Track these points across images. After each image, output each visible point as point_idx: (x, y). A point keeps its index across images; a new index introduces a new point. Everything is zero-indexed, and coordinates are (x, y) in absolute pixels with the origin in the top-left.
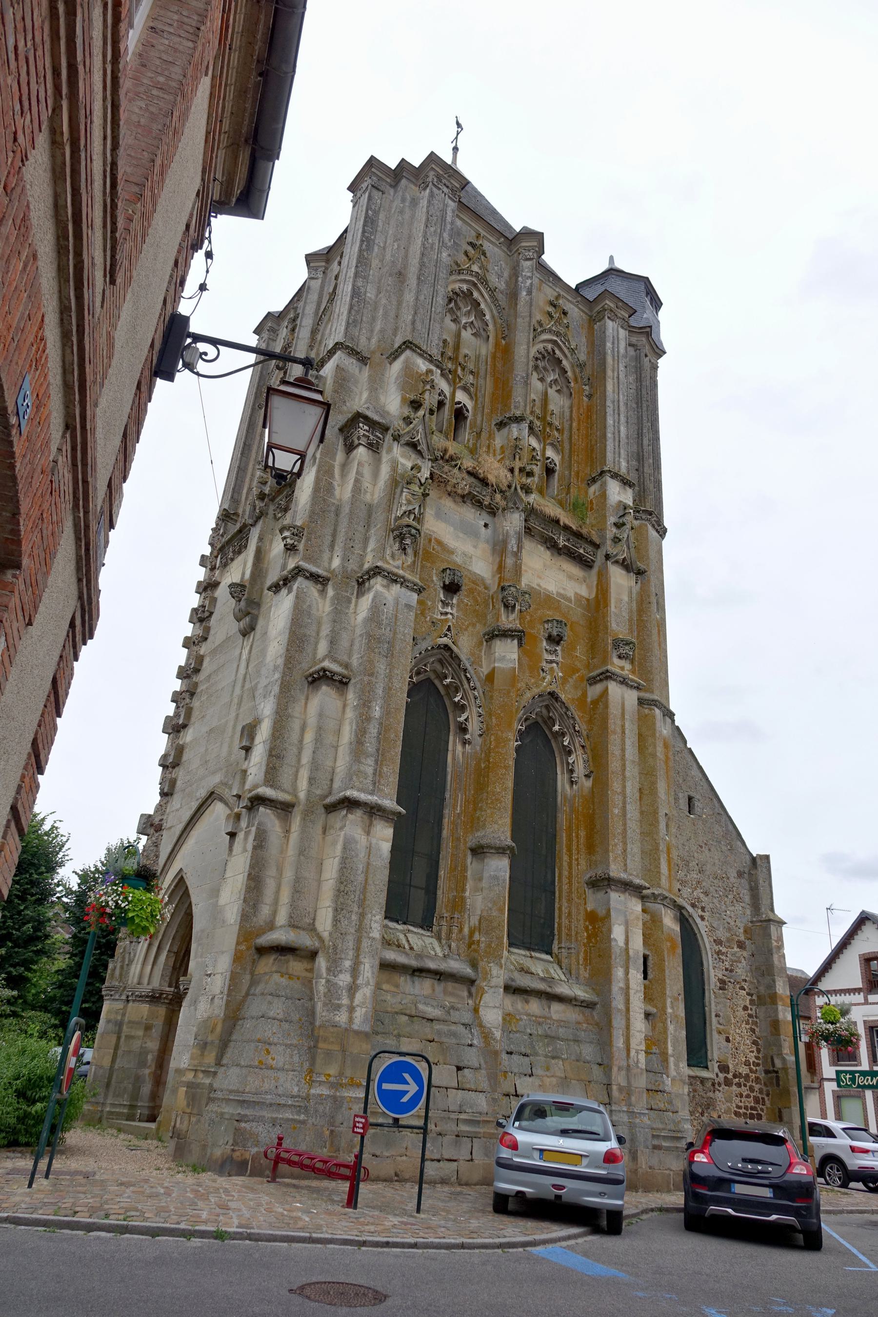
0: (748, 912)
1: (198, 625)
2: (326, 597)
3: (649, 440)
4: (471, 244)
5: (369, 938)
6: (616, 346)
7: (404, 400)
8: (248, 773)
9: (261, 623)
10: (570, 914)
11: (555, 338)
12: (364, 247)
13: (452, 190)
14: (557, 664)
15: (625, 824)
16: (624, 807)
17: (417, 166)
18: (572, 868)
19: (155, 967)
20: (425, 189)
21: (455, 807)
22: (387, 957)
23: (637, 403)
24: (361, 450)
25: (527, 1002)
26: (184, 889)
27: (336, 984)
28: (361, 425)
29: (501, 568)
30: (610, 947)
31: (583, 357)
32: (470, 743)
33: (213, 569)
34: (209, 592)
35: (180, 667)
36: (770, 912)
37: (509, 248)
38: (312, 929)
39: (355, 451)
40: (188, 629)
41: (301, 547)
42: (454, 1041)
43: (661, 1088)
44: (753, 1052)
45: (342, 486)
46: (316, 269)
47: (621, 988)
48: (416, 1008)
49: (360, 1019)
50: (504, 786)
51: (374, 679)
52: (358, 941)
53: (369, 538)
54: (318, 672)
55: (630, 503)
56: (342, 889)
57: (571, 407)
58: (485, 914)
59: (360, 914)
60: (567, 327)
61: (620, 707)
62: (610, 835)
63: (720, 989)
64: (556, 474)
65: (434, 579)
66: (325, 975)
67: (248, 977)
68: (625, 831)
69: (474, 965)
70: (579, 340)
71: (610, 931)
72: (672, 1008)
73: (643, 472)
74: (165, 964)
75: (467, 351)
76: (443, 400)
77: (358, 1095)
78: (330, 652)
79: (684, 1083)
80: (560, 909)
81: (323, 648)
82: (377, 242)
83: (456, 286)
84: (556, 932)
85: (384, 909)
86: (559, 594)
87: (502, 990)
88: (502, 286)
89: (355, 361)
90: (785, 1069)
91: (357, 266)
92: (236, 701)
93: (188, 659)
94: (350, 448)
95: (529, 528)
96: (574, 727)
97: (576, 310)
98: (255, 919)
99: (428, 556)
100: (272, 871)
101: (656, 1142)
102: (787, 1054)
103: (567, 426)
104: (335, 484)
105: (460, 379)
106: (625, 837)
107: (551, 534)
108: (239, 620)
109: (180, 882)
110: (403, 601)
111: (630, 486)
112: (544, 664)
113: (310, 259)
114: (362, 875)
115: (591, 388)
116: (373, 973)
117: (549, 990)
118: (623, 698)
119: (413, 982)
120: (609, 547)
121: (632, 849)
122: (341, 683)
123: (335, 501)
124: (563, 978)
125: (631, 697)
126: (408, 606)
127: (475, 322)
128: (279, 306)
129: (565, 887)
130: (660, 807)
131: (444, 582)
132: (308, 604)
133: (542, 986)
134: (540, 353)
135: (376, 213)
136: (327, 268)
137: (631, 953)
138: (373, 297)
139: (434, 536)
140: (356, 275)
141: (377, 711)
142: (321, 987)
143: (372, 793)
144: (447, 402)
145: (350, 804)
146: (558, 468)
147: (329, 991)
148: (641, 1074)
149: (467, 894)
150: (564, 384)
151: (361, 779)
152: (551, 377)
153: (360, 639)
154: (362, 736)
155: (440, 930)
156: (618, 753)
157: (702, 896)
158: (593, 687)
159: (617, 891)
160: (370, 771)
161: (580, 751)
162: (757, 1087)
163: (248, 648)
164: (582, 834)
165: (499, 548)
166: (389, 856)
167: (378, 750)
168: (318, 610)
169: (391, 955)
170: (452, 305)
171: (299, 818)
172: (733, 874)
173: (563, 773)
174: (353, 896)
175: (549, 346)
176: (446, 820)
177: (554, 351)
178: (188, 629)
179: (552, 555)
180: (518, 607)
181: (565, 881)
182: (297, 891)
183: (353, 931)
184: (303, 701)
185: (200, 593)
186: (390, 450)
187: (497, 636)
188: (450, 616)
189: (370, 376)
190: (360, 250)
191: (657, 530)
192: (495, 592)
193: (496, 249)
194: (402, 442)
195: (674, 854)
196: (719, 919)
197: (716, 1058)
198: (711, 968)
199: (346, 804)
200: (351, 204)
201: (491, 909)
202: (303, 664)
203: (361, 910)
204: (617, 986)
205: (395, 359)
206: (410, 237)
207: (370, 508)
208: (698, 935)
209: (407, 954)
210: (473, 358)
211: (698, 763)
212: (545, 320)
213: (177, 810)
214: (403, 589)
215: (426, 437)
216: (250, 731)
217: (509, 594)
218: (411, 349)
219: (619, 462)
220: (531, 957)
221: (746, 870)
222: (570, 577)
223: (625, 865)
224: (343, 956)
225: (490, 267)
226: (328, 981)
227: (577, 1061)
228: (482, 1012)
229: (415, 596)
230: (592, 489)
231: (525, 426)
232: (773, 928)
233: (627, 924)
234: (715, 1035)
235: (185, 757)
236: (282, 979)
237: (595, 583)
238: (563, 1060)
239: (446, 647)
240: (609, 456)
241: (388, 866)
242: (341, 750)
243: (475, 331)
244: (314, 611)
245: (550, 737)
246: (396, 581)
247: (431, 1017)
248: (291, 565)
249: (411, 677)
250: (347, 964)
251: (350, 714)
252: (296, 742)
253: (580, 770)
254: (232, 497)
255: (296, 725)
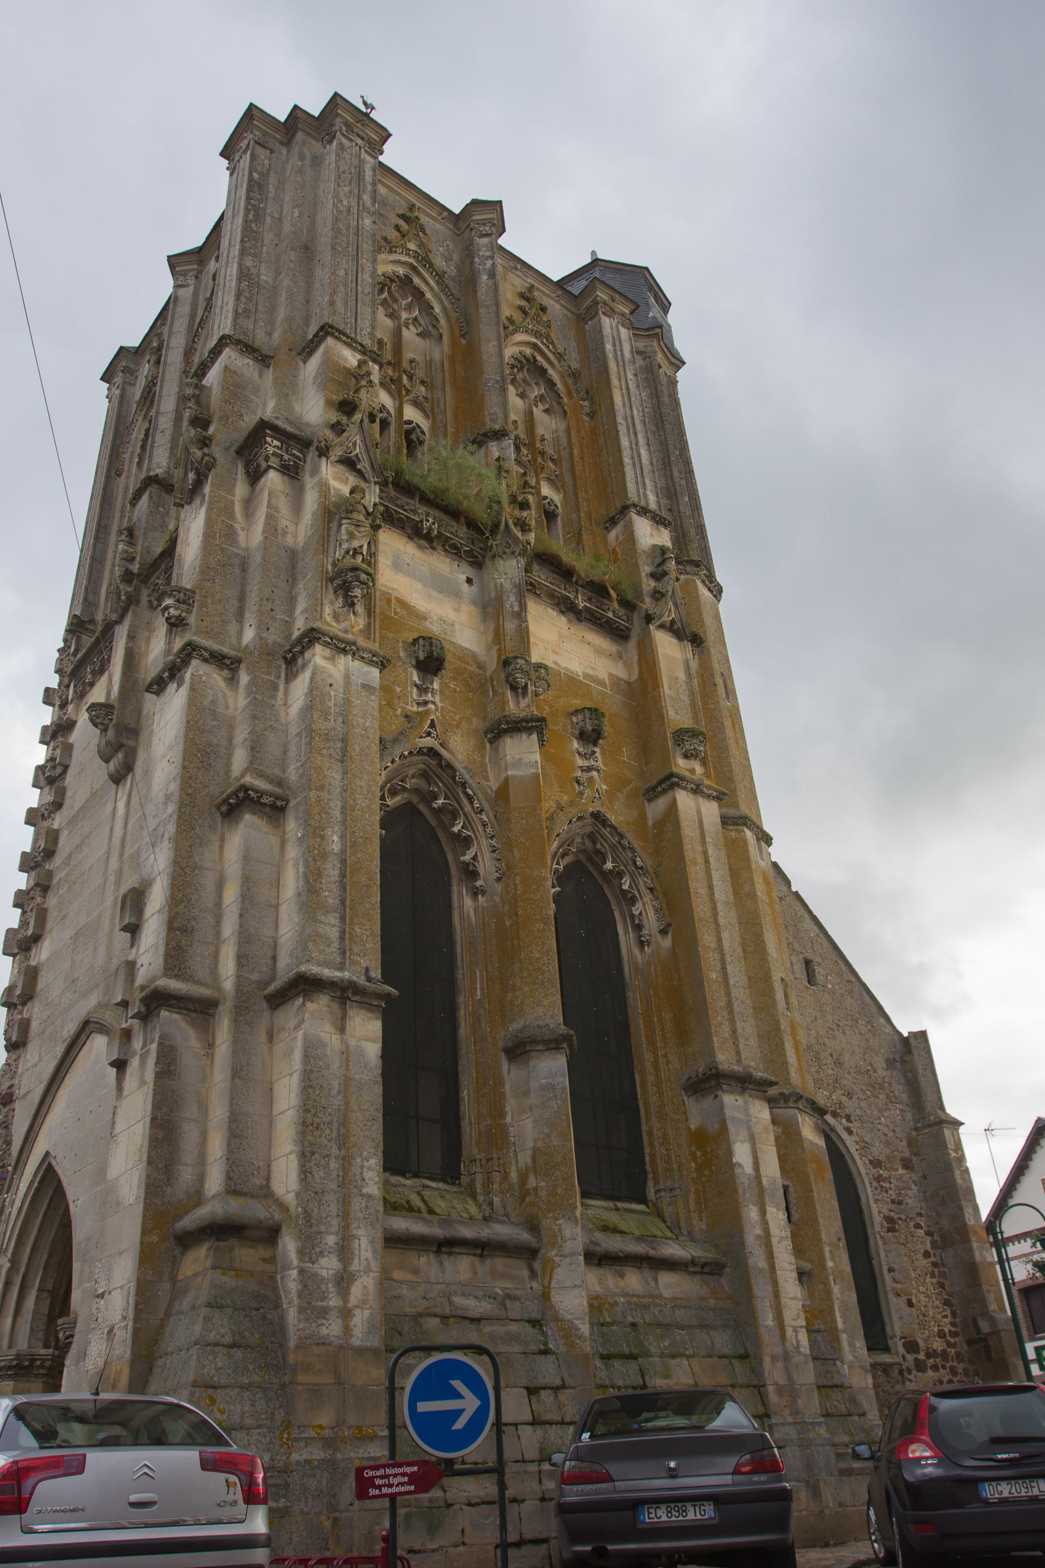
0: (909, 1116)
1: (47, 789)
2: (237, 688)
3: (681, 473)
4: (402, 216)
5: (363, 1196)
6: (618, 348)
7: (329, 403)
8: (138, 965)
9: (141, 756)
10: (665, 1137)
11: (534, 340)
12: (251, 217)
13: (370, 143)
14: (598, 771)
15: (728, 994)
16: (724, 969)
17: (316, 115)
18: (658, 1070)
19: (19, 1319)
20: (330, 142)
21: (473, 990)
22: (395, 1226)
23: (656, 425)
24: (272, 476)
25: (622, 1276)
26: (55, 1184)
27: (316, 1274)
28: (269, 439)
29: (498, 636)
30: (733, 1176)
31: (575, 365)
32: (484, 893)
33: (63, 706)
34: (60, 739)
35: (24, 853)
36: (939, 1112)
37: (455, 225)
38: (266, 1193)
39: (263, 480)
40: (33, 798)
41: (192, 619)
42: (517, 1348)
43: (836, 1381)
44: (946, 1316)
45: (247, 529)
46: (185, 274)
47: (758, 1236)
48: (451, 1303)
49: (363, 1325)
50: (542, 950)
51: (324, 795)
52: (345, 1202)
53: (296, 596)
54: (235, 794)
55: (669, 544)
56: (309, 1120)
57: (568, 431)
58: (540, 1145)
59: (344, 1159)
60: (549, 326)
61: (697, 825)
62: (710, 1012)
63: (889, 1230)
64: (559, 519)
65: (402, 654)
66: (295, 1262)
67: (167, 1286)
68: (729, 1004)
69: (534, 1228)
70: (566, 342)
71: (730, 1153)
72: (833, 1259)
73: (679, 512)
74: (35, 1312)
75: (412, 356)
76: (386, 419)
77: (372, 1454)
78: (251, 763)
79: (866, 1371)
80: (650, 1133)
81: (239, 760)
82: (268, 211)
83: (389, 268)
84: (648, 1168)
85: (381, 1148)
86: (586, 675)
87: (582, 1258)
88: (452, 270)
89: (251, 362)
90: (996, 1333)
91: (242, 241)
92: (112, 879)
93: (35, 840)
94: (254, 476)
95: (531, 584)
96: (635, 862)
97: (558, 306)
98: (169, 1190)
99: (389, 622)
100: (190, 1111)
101: (843, 1465)
102: (994, 1311)
103: (565, 454)
104: (238, 526)
105: (408, 391)
106: (731, 1012)
107: (565, 593)
108: (107, 761)
109: (48, 1175)
110: (357, 680)
111: (665, 526)
112: (579, 773)
113: (175, 262)
114: (341, 1097)
115: (592, 404)
116: (374, 1252)
117: (652, 1252)
118: (699, 813)
119: (441, 1264)
120: (648, 604)
121: (743, 1029)
122: (274, 809)
123: (239, 552)
124: (669, 1234)
125: (711, 811)
126: (366, 687)
127: (419, 318)
128: (135, 341)
129: (653, 1099)
130: (773, 968)
131: (417, 658)
132: (210, 698)
133: (639, 1249)
134: (516, 359)
135: (264, 175)
136: (200, 272)
137: (765, 1181)
138: (270, 281)
139: (394, 594)
140: (243, 252)
141: (335, 842)
142: (291, 1283)
143: (341, 967)
144: (393, 421)
145: (305, 985)
146: (560, 510)
147: (305, 1286)
148: (806, 1362)
149: (508, 1119)
150: (555, 404)
151: (321, 947)
152: (535, 392)
153: (297, 739)
154: (315, 881)
155: (473, 1181)
156: (703, 891)
157: (844, 1099)
158: (653, 804)
159: (731, 1092)
160: (334, 933)
161: (648, 897)
162: (960, 1367)
163: (125, 797)
164: (667, 1016)
165: (490, 609)
166: (380, 1063)
167: (343, 902)
168: (227, 707)
169: (401, 1224)
170: (385, 295)
171: (226, 1022)
172: (880, 1064)
173: (626, 932)
174: (328, 1131)
175: (528, 351)
176: (462, 1012)
177: (534, 357)
178: (33, 798)
179: (570, 621)
180: (531, 688)
181: (651, 1089)
182: (235, 1136)
183: (333, 1186)
184: (217, 844)
185: (47, 743)
186: (316, 470)
187: (505, 731)
188: (431, 706)
189: (275, 379)
190: (246, 221)
191: (709, 589)
192: (493, 672)
193: (438, 226)
194: (333, 458)
195: (802, 1036)
196: (872, 1130)
197: (898, 1332)
198: (872, 1202)
199: (301, 987)
200: (228, 173)
201: (548, 1136)
202: (211, 788)
203: (343, 1152)
204: (752, 1234)
205: (311, 354)
206: (315, 203)
207: (293, 557)
208: (847, 1157)
209: (425, 1220)
210: (422, 365)
211: (810, 912)
212: (518, 317)
213: (35, 1066)
214: (357, 663)
215: (367, 451)
216: (134, 901)
217: (513, 668)
218: (332, 335)
219: (646, 496)
220: (617, 1209)
221: (897, 1057)
222: (599, 652)
223: (738, 1053)
224: (322, 1228)
225: (432, 246)
226: (302, 1271)
227: (710, 1356)
228: (556, 1297)
229: (375, 672)
230: (613, 535)
231: (509, 443)
232: (947, 1132)
233: (752, 1139)
234: (893, 1300)
235: (41, 984)
236: (225, 1279)
237: (636, 658)
238: (688, 1357)
239: (432, 752)
240: (631, 487)
241: (380, 1079)
242: (284, 910)
243: (420, 330)
244: (221, 709)
245: (601, 881)
246: (344, 651)
247: (477, 1316)
248: (178, 644)
249: (383, 798)
250: (331, 1240)
251: (293, 852)
252: (210, 905)
253: (651, 922)
254: (85, 599)
255: (209, 880)
